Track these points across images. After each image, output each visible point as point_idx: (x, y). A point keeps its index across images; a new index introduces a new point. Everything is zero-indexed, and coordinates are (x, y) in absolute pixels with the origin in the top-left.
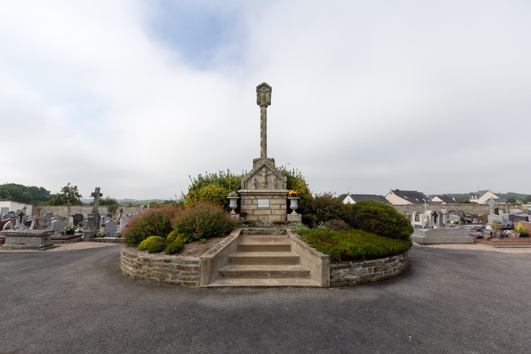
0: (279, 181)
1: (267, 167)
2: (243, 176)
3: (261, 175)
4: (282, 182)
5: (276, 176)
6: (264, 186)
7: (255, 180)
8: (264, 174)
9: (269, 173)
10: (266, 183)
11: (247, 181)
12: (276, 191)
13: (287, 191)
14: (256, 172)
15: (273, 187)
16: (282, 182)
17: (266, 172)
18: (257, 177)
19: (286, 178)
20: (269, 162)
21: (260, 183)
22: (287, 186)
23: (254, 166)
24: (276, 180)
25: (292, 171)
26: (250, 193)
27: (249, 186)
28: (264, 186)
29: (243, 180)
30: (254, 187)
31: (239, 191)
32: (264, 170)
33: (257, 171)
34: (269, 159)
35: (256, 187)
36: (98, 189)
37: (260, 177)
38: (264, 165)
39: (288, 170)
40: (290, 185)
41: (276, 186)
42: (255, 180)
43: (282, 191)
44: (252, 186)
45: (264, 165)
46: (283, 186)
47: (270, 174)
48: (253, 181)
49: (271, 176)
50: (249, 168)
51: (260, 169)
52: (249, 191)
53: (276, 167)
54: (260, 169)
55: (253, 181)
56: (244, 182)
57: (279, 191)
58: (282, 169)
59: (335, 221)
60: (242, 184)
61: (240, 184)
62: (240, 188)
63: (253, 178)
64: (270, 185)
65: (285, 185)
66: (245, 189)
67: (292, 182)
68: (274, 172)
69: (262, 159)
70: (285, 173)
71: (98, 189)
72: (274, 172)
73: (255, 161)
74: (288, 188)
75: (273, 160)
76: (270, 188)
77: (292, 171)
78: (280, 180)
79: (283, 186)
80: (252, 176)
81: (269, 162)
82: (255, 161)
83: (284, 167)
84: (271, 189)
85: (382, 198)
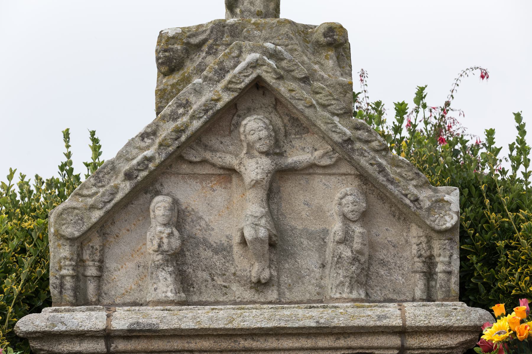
0: (387, 231)
1: (278, 103)
2: (65, 184)
3: (230, 173)
4: (415, 233)
5: (363, 177)
6: (256, 270)
7: (179, 218)
8: (255, 168)
9: (298, 155)
10: (276, 245)
11: (102, 227)
12: (368, 316)
13: (463, 314)
14: (183, 151)
15: (334, 281)
16: (415, 233)
17: (275, 150)
18: (191, 194)
19: (453, 197)
20: (302, 60)
21: (223, 250)
22: (466, 273)
23: (163, 96)
24: (364, 217)
25: (506, 137)
26: (130, 335)
27: (122, 276)
28: (256, 270)
29: (63, 223)
30: (165, 286)
31: (29, 323)
32: (254, 126)
33: (198, 139)
34: (303, 32)
35: (184, 282)
36: (68, 130)
37: (219, 195)
38: (258, 85)
39: (472, 130)
40: (491, 257)
41: (365, 275)
42: (179, 218)
43: (418, 314)
44: (145, 272)
45: (258, 85)
46: (429, 274)
47: (311, 168)
48: (156, 231)
49: (319, 182)
50: (124, 111)
51: (223, 120)
52: (122, 319)
53: (365, 102)
54: (223, 120)
55: (156, 231)
56: (79, 243)
57: (392, 315)
58: (421, 121)
59: (208, 32)
60: (60, 255)
61: (42, 257)
62: (37, 298)
63: (160, 206)
64: (308, 261)
65: (448, 261)
66: (80, 300)
67: (506, 232)
68: (345, 149)
69: (235, 31)
70: (443, 157)
71: (68, 130)
72: (345, 149)
73: (176, 55)
74: (473, 292)
75: (334, 41)
76: (309, 289)
77: (506, 137)
78: (404, 213)
79: (429, 274)
80: (146, 184)
81: (302, 60)
82: (176, 55)
83: (435, 99)
84: (319, 300)
85: (183, 69)
